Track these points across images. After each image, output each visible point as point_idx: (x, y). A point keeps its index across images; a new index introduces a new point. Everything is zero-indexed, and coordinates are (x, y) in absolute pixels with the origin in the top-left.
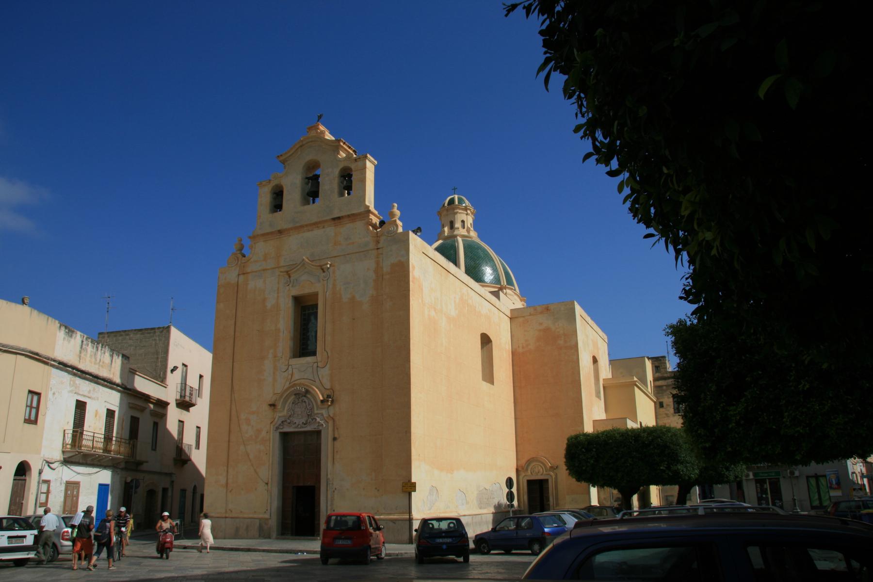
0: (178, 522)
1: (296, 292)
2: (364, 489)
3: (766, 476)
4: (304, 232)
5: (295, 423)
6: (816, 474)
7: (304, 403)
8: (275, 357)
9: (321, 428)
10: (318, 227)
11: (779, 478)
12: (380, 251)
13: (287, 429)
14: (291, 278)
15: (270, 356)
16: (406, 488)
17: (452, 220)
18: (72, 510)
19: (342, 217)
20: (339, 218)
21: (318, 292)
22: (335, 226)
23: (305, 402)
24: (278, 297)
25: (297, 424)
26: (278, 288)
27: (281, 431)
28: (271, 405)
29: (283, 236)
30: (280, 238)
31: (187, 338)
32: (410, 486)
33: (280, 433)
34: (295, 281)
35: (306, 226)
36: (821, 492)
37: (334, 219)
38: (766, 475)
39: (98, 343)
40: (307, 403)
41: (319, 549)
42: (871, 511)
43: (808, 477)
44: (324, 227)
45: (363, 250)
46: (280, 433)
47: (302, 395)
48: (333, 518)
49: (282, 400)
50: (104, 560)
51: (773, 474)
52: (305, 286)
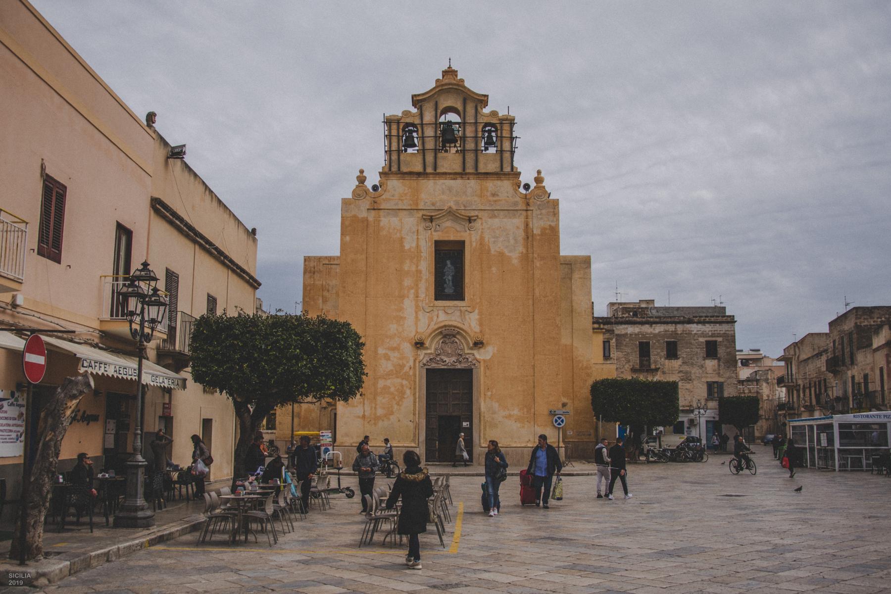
0: (468, 423)
1: (437, 236)
5: (445, 361)
9: (473, 367)
10: (462, 177)
11: (426, 461)
12: (529, 212)
13: (434, 365)
15: (412, 296)
17: (553, 224)
23: (456, 342)
24: (418, 238)
25: (447, 362)
26: (418, 231)
27: (428, 367)
28: (416, 344)
31: (340, 222)
33: (427, 369)
35: (450, 174)
41: (484, 472)
42: (889, 412)
44: (468, 179)
45: (512, 209)
46: (427, 369)
47: (448, 334)
48: (261, 485)
49: (429, 339)
50: (357, 503)
52: (450, 231)
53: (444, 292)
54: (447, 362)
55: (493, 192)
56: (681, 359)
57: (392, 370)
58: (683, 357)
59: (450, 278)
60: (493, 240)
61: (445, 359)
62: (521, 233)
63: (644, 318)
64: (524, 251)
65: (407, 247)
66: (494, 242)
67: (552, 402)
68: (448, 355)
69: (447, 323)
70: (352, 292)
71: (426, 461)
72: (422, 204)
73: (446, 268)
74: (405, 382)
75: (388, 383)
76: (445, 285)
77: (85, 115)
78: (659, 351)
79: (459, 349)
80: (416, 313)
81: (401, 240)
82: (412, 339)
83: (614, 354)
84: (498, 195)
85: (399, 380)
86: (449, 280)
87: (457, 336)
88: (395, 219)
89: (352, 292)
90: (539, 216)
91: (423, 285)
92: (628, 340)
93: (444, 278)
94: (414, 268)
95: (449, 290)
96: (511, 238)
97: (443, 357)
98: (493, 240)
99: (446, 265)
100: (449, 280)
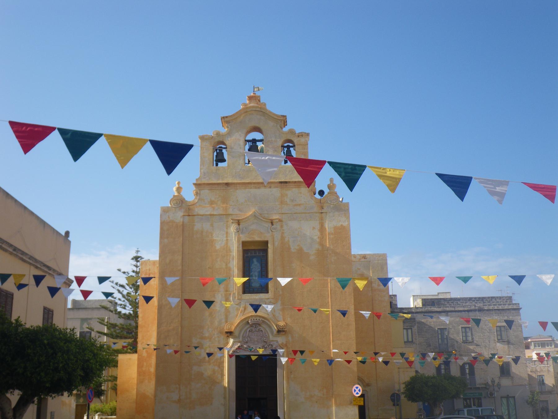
2: (317, 402)
3: (472, 396)
4: (251, 188)
6: (508, 395)
7: (261, 332)
8: (227, 291)
14: (240, 226)
16: (357, 402)
18: (473, 415)
19: (289, 182)
20: (286, 182)
21: (268, 241)
22: (281, 188)
29: (229, 188)
30: (226, 189)
32: (359, 401)
34: (244, 229)
36: (510, 410)
37: (281, 182)
38: (472, 395)
39: (129, 278)
40: (264, 332)
43: (502, 397)
51: (477, 395)
59: (257, 274)
84: (295, 201)
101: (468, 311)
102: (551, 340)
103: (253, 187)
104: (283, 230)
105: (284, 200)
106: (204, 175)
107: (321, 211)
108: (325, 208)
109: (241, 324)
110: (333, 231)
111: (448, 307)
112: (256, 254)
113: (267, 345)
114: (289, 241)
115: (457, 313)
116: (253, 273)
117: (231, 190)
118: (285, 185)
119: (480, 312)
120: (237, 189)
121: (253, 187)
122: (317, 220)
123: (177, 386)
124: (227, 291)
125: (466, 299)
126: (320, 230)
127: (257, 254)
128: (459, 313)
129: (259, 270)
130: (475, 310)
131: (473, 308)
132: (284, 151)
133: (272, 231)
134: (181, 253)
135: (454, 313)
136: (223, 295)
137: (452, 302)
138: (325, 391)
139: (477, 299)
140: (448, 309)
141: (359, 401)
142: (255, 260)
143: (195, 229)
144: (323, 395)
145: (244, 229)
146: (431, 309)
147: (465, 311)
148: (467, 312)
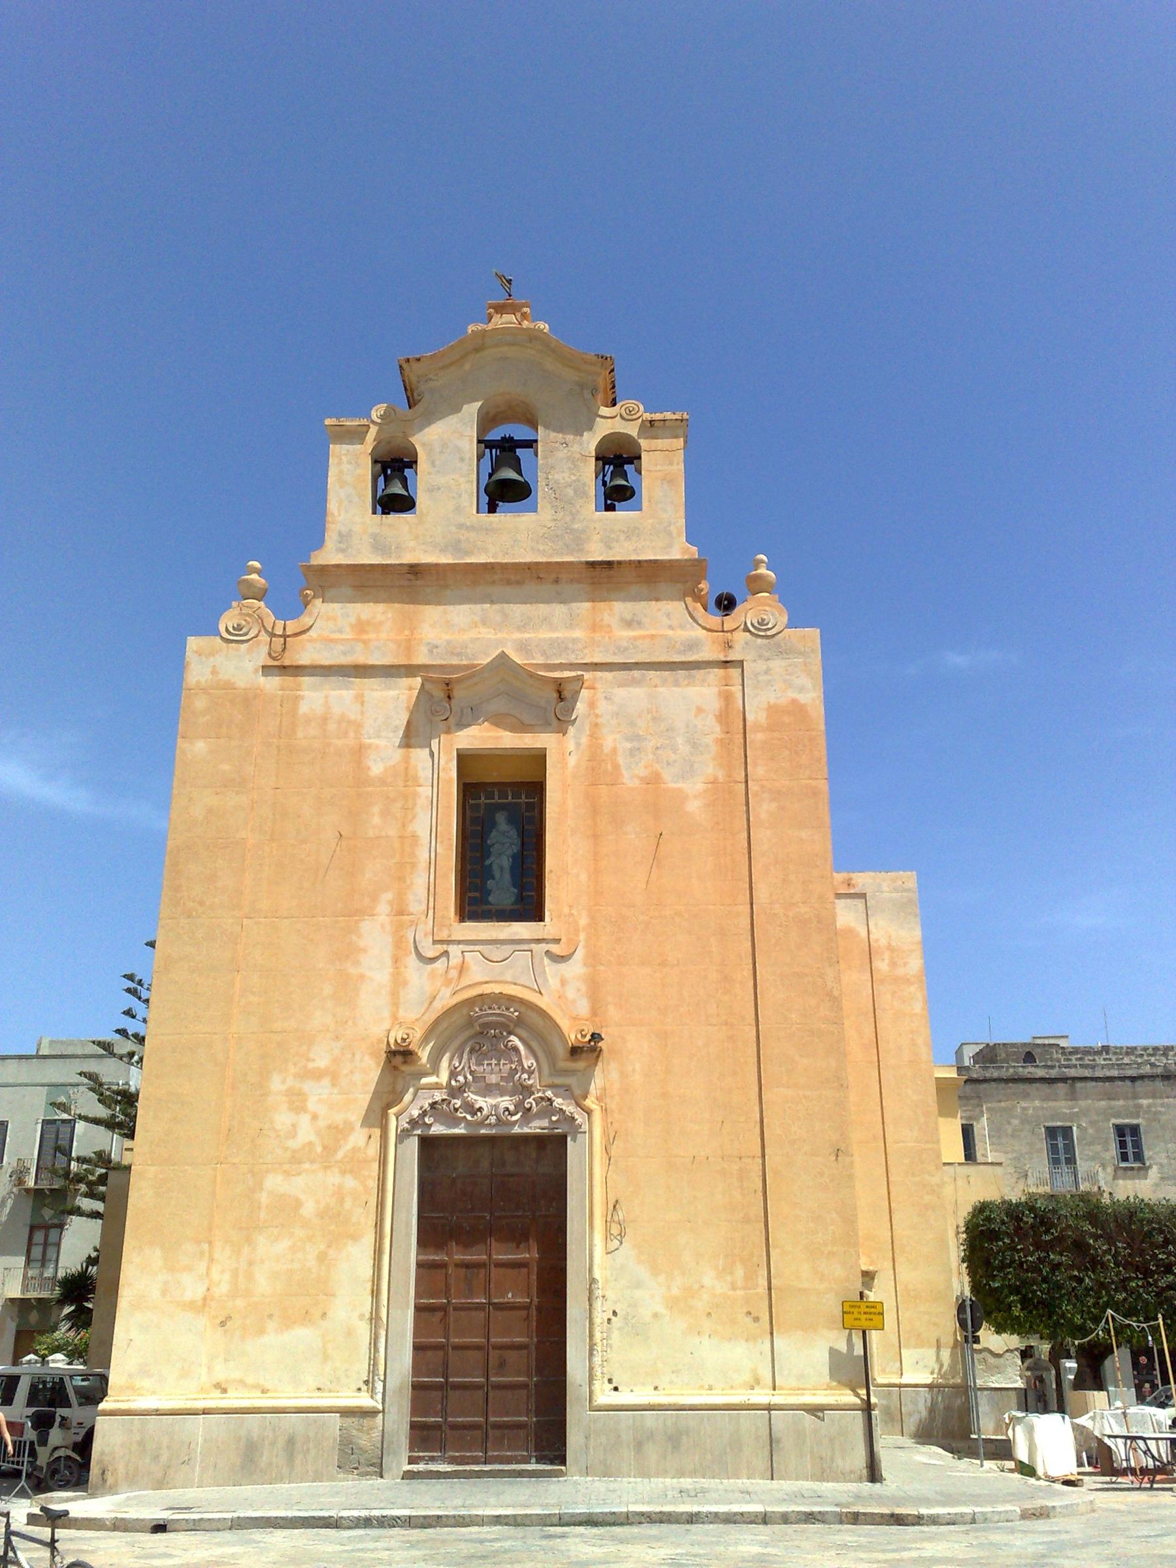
4: (493, 582)
5: (480, 1109)
13: (438, 1129)
15: (383, 908)
22: (593, 583)
25: (485, 1112)
29: (419, 583)
32: (865, 1313)
53: (488, 903)
54: (485, 1112)
55: (629, 617)
56: (1155, 1169)
57: (310, 1143)
58: (1161, 1165)
59: (506, 862)
60: (628, 745)
61: (480, 1102)
62: (710, 728)
63: (1052, 1067)
64: (721, 775)
65: (376, 769)
66: (632, 752)
67: (531, 348)
68: (487, 1090)
69: (487, 989)
70: (201, 903)
71: (410, 1452)
72: (424, 650)
73: (494, 833)
74: (350, 1182)
75: (297, 1186)
76: (490, 884)
77: (396, 1188)
78: (1098, 1148)
79: (523, 1071)
80: (396, 960)
81: (360, 751)
82: (380, 1041)
83: (985, 1149)
84: (639, 623)
85: (333, 1178)
86: (502, 869)
87: (518, 1031)
88: (344, 693)
89: (201, 903)
90: (762, 678)
91: (420, 882)
92: (1016, 1122)
93: (488, 862)
94: (392, 832)
95: (502, 892)
96: (680, 740)
97: (471, 1097)
98: (628, 745)
99: (494, 824)
100: (502, 869)
101: (1133, 1079)
102: (827, 1410)
103: (501, 580)
104: (597, 716)
105: (602, 620)
106: (340, 543)
107: (726, 656)
108: (738, 647)
109: (445, 1025)
110: (763, 721)
111: (1075, 1066)
112: (507, 799)
113: (534, 1099)
114: (614, 751)
115: (1101, 1084)
116: (492, 859)
117: (429, 590)
118: (606, 573)
119: (1166, 1083)
120: (446, 586)
121: (501, 580)
122: (709, 686)
123: (206, 1246)
124: (401, 912)
125: (1118, 1051)
126: (721, 715)
127: (510, 798)
128: (1107, 1083)
129: (515, 849)
130: (1152, 1077)
131: (1147, 1069)
132: (604, 476)
133: (559, 719)
134: (462, 1313)
135: (1094, 1084)
136: (388, 927)
137: (1080, 1059)
138: (740, 1272)
139: (1150, 1051)
140: (1073, 1073)
141: (865, 1313)
142: (501, 818)
143: (304, 708)
144: (734, 1287)
145: (465, 710)
146: (1026, 1070)
147: (1122, 1079)
148: (1128, 1083)
